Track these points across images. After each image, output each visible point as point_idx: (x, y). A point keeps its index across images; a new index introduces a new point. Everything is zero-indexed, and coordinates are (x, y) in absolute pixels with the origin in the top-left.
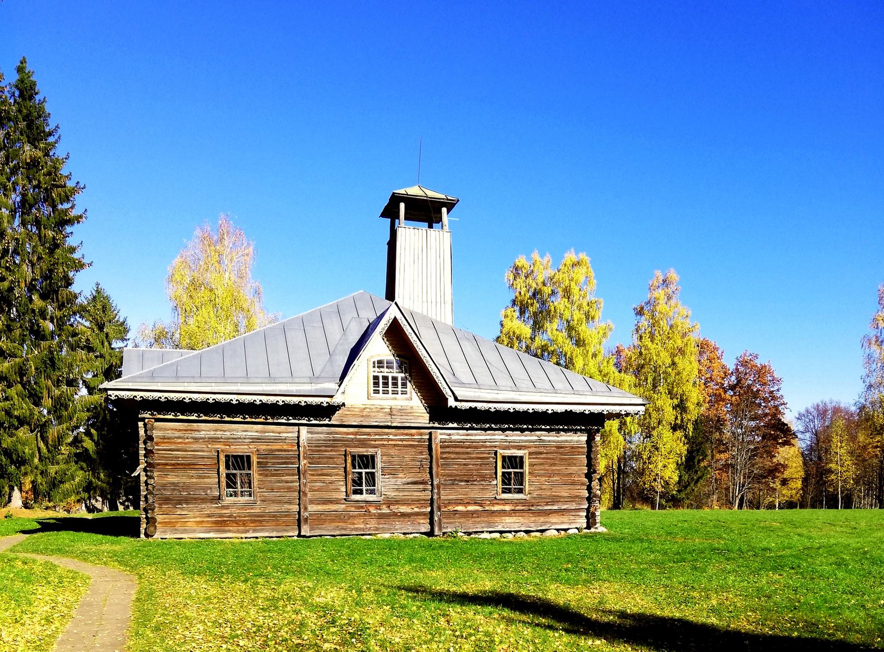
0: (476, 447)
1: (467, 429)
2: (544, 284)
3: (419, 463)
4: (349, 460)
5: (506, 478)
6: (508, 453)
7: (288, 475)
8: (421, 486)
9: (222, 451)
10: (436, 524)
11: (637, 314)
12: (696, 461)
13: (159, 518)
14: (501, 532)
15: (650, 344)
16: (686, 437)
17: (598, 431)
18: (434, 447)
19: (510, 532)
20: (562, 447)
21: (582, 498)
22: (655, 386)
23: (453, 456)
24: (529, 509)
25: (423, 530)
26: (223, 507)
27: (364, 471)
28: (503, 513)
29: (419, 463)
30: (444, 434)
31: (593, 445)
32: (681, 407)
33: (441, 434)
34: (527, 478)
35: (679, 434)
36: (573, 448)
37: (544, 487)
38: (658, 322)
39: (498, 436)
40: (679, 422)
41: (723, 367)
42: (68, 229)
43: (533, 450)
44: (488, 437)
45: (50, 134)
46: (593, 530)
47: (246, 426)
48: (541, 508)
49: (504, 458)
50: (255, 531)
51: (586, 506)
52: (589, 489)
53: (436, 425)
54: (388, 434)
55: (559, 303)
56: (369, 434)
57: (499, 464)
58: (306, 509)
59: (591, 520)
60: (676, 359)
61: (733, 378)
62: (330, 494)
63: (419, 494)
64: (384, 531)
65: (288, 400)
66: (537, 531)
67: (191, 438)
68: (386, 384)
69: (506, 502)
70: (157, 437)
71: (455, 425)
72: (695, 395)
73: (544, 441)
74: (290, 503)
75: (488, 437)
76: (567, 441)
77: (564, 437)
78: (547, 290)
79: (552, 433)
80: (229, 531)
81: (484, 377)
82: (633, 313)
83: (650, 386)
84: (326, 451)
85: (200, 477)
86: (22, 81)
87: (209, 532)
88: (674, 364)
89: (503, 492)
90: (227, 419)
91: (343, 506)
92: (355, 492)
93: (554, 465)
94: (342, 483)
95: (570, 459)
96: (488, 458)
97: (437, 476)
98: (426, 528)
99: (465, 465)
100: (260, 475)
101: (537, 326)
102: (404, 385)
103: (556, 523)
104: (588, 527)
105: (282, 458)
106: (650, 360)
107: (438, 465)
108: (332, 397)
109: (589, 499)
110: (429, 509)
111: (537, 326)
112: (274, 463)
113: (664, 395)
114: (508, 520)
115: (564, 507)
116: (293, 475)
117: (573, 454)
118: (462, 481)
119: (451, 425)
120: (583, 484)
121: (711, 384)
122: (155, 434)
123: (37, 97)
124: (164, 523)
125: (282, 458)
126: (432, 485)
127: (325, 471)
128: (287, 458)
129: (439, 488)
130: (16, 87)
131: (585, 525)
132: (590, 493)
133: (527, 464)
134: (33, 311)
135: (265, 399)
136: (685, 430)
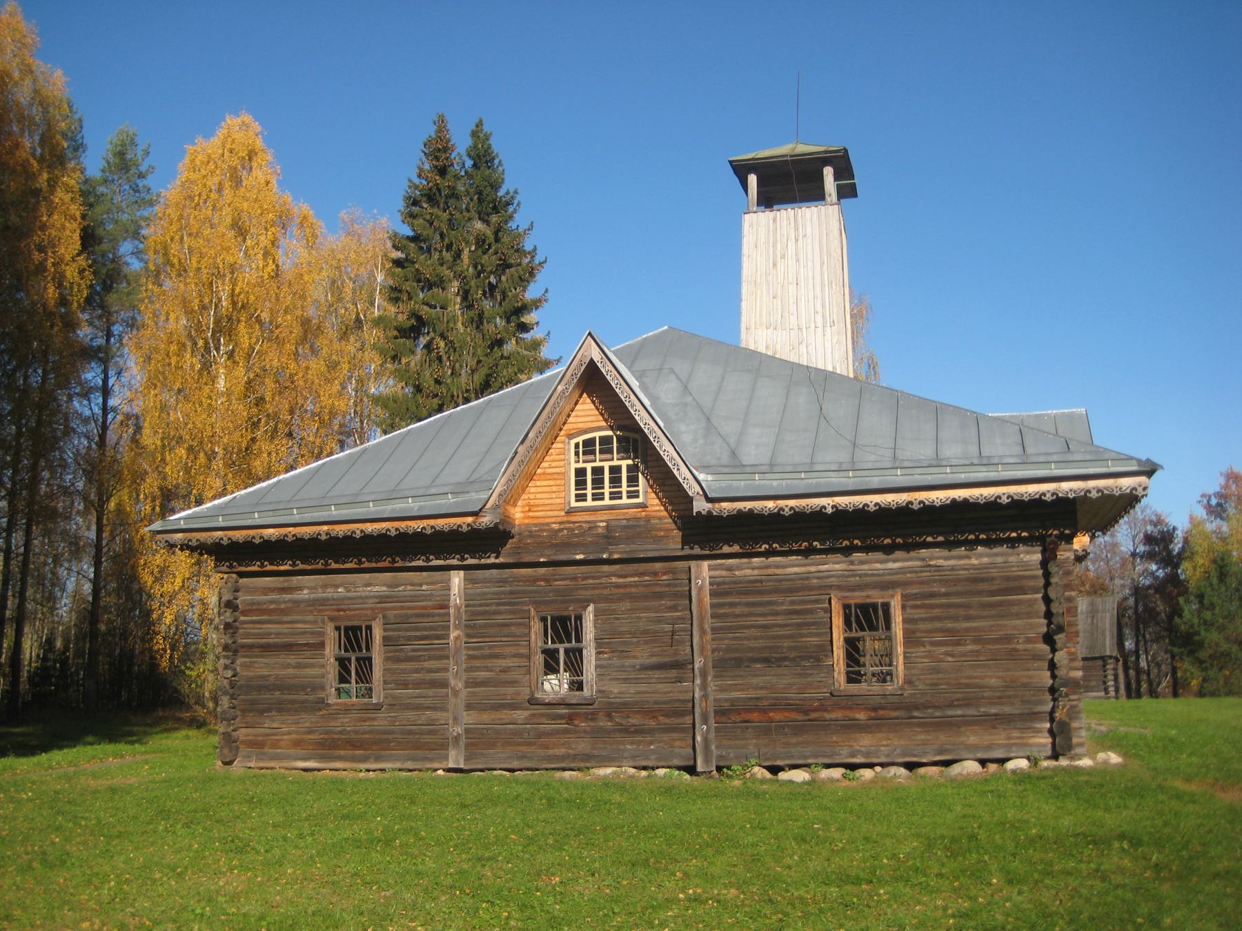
0: (791, 591)
3: (668, 627)
6: (858, 597)
7: (431, 658)
8: (673, 673)
19: (871, 766)
21: (1039, 689)
23: (738, 610)
28: (853, 727)
39: (834, 566)
42: (527, 318)
44: (813, 569)
45: (508, 204)
46: (1064, 762)
47: (367, 576)
49: (846, 607)
50: (378, 759)
52: (1052, 666)
53: (697, 551)
57: (838, 622)
62: (503, 690)
67: (289, 601)
68: (598, 483)
71: (736, 548)
75: (813, 569)
77: (980, 558)
79: (956, 552)
90: (334, 566)
91: (526, 713)
93: (968, 618)
95: (1000, 604)
96: (811, 611)
102: (633, 480)
107: (703, 632)
108: (475, 514)
109: (1052, 690)
110: (688, 719)
112: (410, 638)
119: (726, 549)
120: (1037, 657)
122: (243, 599)
124: (253, 744)
125: (425, 629)
128: (431, 629)
130: (469, 156)
132: (1054, 677)
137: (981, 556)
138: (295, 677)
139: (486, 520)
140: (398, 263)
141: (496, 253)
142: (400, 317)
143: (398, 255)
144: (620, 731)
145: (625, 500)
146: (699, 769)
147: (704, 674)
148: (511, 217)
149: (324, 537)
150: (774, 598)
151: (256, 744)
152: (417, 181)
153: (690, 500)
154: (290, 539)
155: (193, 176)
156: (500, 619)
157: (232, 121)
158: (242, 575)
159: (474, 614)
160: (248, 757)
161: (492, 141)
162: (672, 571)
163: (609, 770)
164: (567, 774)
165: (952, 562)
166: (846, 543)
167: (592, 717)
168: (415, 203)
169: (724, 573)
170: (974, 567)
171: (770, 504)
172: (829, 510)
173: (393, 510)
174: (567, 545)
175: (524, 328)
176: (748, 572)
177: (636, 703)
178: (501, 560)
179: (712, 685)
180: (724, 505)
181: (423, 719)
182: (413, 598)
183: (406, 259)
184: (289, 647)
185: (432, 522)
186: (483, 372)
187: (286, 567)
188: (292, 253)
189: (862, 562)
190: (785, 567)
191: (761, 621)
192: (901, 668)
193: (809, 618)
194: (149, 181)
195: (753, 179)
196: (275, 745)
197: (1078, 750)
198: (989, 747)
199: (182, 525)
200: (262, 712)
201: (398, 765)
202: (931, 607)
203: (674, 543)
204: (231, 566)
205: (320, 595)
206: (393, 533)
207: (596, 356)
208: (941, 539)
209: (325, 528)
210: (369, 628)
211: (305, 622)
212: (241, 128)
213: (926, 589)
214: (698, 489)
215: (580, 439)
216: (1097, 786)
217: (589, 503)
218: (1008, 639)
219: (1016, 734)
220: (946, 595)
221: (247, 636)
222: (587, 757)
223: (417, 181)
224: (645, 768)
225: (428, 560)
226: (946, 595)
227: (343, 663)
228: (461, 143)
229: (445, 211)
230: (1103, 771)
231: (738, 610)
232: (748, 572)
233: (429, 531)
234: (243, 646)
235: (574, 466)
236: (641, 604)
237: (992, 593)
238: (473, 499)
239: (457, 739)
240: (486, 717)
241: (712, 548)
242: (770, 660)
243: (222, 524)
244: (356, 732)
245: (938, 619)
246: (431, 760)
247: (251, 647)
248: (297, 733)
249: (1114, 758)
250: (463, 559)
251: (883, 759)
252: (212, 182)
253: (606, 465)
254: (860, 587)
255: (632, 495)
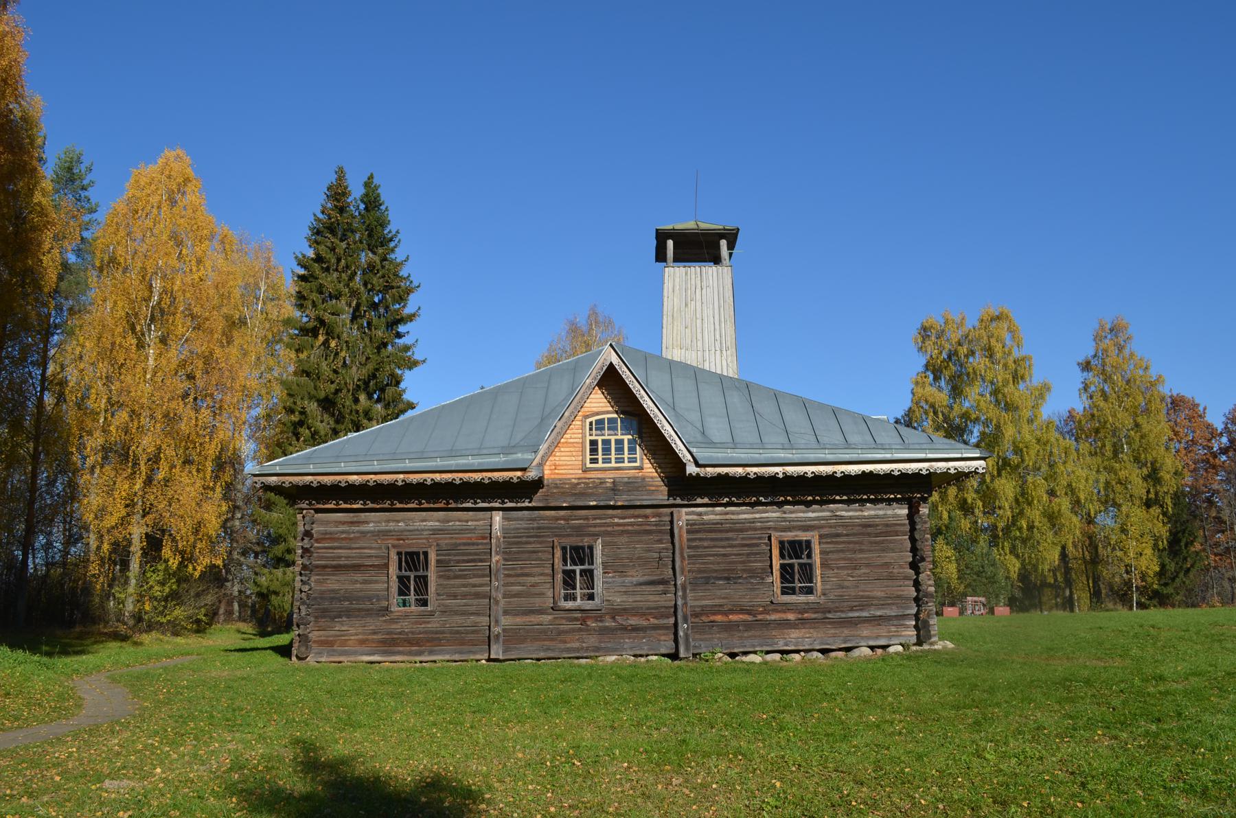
0: (741, 530)
1: (725, 505)
2: (960, 344)
3: (656, 555)
4: (558, 553)
5: (786, 572)
6: (789, 536)
8: (661, 588)
9: (394, 546)
10: (681, 641)
11: (1083, 370)
12: (1183, 544)
13: (314, 636)
14: (782, 652)
15: (1102, 404)
16: (1164, 514)
17: (925, 500)
18: (676, 531)
19: (798, 652)
20: (870, 526)
21: (907, 599)
22: (1116, 453)
23: (706, 544)
24: (821, 616)
25: (663, 651)
26: (393, 621)
27: (578, 568)
28: (785, 625)
29: (656, 555)
30: (693, 513)
31: (917, 520)
32: (1153, 477)
33: (687, 514)
34: (818, 572)
35: (1156, 510)
36: (887, 525)
37: (846, 583)
38: (1110, 377)
39: (772, 514)
40: (1152, 496)
41: (1208, 426)
42: (402, 328)
43: (825, 531)
44: (757, 516)
45: (391, 240)
46: (926, 647)
47: (424, 514)
48: (843, 615)
49: (782, 543)
50: (431, 653)
51: (914, 611)
52: (917, 584)
53: (679, 501)
54: (612, 517)
55: (978, 362)
56: (587, 518)
57: (776, 552)
58: (497, 621)
59: (923, 632)
60: (1139, 420)
61: (1224, 440)
62: (532, 600)
63: (657, 598)
64: (609, 652)
65: (466, 476)
66: (840, 650)
68: (607, 450)
69: (787, 607)
70: (318, 532)
71: (706, 500)
72: (1169, 463)
73: (842, 517)
74: (477, 614)
75: (757, 516)
76: (877, 516)
77: (870, 511)
78: (963, 350)
79: (880, 506)
80: (399, 653)
81: (746, 433)
82: (1078, 369)
83: (1109, 454)
84: (530, 543)
85: (365, 582)
86: (367, 195)
87: (373, 654)
88: (1137, 425)
89: (783, 593)
90: (399, 506)
91: (550, 617)
92: (566, 598)
93: (861, 551)
94: (548, 586)
95: (882, 542)
96: (757, 545)
97: (682, 573)
98: (668, 647)
99: (724, 555)
100: (440, 577)
101: (956, 392)
102: (632, 450)
103: (868, 638)
104: (919, 643)
105: (470, 554)
106: (1105, 422)
107: (683, 558)
108: (524, 470)
109: (917, 600)
110: (672, 620)
111: (956, 392)
112: (458, 561)
113: (1128, 465)
114: (794, 634)
115: (879, 613)
116: (483, 576)
117: (887, 534)
118: (720, 579)
119: (699, 501)
120: (906, 578)
121: (1195, 448)
122: (316, 529)
123: (383, 207)
125: (470, 554)
126: (675, 585)
127: (527, 571)
128: (476, 554)
129: (684, 588)
130: (362, 201)
131: (914, 640)
132: (918, 590)
133: (817, 551)
134: (357, 412)
135: (437, 477)
136: (1162, 506)
137: (869, 509)
138: (361, 591)
139: (532, 474)
140: (302, 278)
141: (383, 277)
142: (305, 319)
143: (302, 272)
144: (621, 629)
145: (626, 464)
146: (682, 655)
147: (684, 588)
148: (393, 250)
149: (400, 483)
150: (730, 535)
151: (327, 643)
152: (321, 216)
153: (683, 466)
154: (371, 484)
155: (139, 194)
156: (530, 547)
157: (170, 154)
158: (318, 511)
159: (509, 543)
160: (320, 654)
161: (379, 191)
162: (659, 515)
163: (614, 658)
164: (583, 661)
165: (851, 514)
166: (782, 498)
167: (599, 619)
168: (318, 233)
169: (695, 517)
170: (864, 517)
171: (740, 470)
172: (781, 476)
173: (457, 465)
174: (582, 494)
175: (399, 335)
176: (712, 517)
177: (633, 609)
178: (533, 504)
179: (690, 595)
180: (708, 469)
181: (469, 623)
182: (461, 531)
183: (312, 276)
184: (356, 568)
185: (489, 475)
186: (371, 366)
187: (331, 506)
188: (215, 259)
189: (791, 512)
190: (738, 513)
191: (722, 551)
192: (819, 584)
193: (755, 550)
194: (90, 193)
195: (670, 243)
196: (344, 643)
197: (933, 639)
198: (877, 637)
199: (278, 470)
200: (333, 618)
201: (447, 657)
202: (837, 543)
203: (662, 495)
204: (310, 504)
205: (383, 526)
206: (458, 482)
207: (615, 360)
208: (845, 497)
209: (402, 476)
210: (426, 554)
211: (371, 548)
212: (175, 159)
213: (833, 531)
214: (690, 457)
215: (593, 419)
216: (940, 658)
217: (600, 465)
218: (887, 565)
219: (893, 629)
220: (847, 535)
221: (321, 558)
222: (597, 649)
223: (321, 216)
224: (641, 656)
225: (476, 503)
226: (847, 535)
227: (403, 581)
228: (356, 191)
229: (342, 240)
230: (945, 651)
231: (706, 544)
232: (712, 517)
233: (487, 481)
234: (317, 567)
235: (588, 438)
236: (636, 539)
237: (877, 535)
238: (520, 457)
239: (498, 636)
240: (518, 620)
241: (689, 500)
242: (729, 578)
243: (312, 471)
244: (413, 633)
245: (842, 551)
246: (474, 653)
247: (325, 567)
248: (364, 634)
249: (950, 645)
250: (503, 503)
251: (807, 647)
252: (154, 200)
253: (613, 438)
254: (789, 529)
255: (631, 460)
